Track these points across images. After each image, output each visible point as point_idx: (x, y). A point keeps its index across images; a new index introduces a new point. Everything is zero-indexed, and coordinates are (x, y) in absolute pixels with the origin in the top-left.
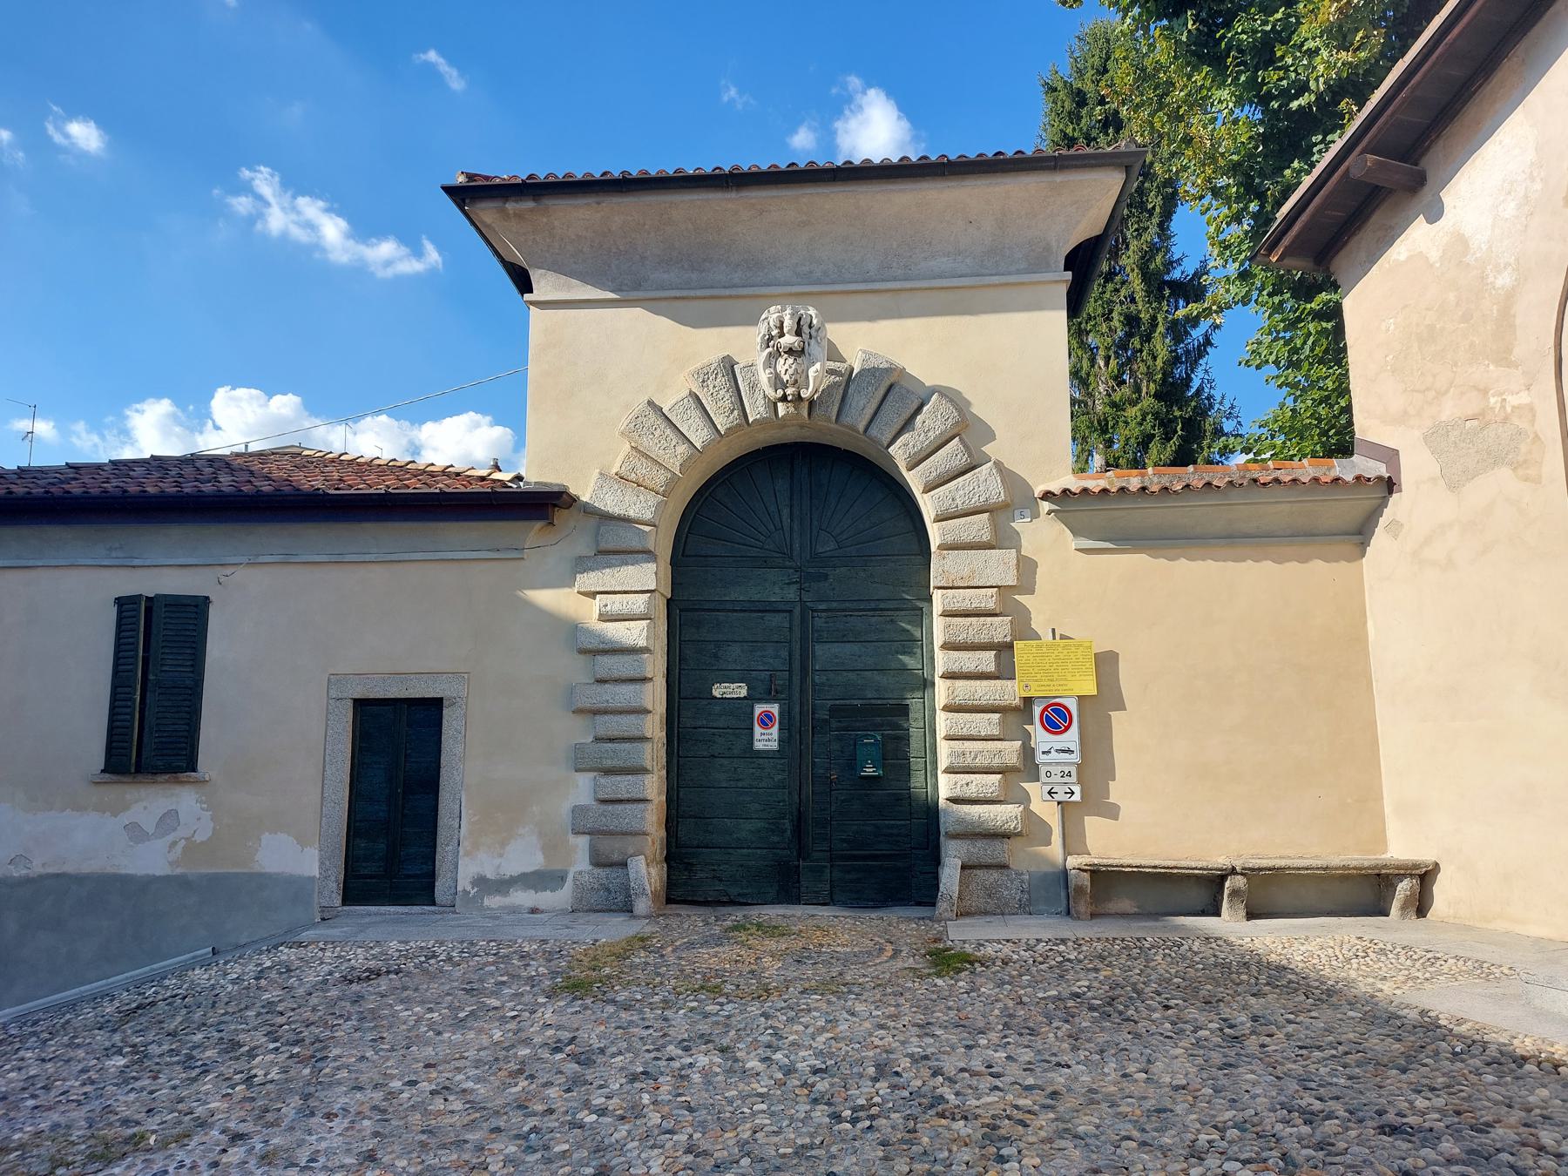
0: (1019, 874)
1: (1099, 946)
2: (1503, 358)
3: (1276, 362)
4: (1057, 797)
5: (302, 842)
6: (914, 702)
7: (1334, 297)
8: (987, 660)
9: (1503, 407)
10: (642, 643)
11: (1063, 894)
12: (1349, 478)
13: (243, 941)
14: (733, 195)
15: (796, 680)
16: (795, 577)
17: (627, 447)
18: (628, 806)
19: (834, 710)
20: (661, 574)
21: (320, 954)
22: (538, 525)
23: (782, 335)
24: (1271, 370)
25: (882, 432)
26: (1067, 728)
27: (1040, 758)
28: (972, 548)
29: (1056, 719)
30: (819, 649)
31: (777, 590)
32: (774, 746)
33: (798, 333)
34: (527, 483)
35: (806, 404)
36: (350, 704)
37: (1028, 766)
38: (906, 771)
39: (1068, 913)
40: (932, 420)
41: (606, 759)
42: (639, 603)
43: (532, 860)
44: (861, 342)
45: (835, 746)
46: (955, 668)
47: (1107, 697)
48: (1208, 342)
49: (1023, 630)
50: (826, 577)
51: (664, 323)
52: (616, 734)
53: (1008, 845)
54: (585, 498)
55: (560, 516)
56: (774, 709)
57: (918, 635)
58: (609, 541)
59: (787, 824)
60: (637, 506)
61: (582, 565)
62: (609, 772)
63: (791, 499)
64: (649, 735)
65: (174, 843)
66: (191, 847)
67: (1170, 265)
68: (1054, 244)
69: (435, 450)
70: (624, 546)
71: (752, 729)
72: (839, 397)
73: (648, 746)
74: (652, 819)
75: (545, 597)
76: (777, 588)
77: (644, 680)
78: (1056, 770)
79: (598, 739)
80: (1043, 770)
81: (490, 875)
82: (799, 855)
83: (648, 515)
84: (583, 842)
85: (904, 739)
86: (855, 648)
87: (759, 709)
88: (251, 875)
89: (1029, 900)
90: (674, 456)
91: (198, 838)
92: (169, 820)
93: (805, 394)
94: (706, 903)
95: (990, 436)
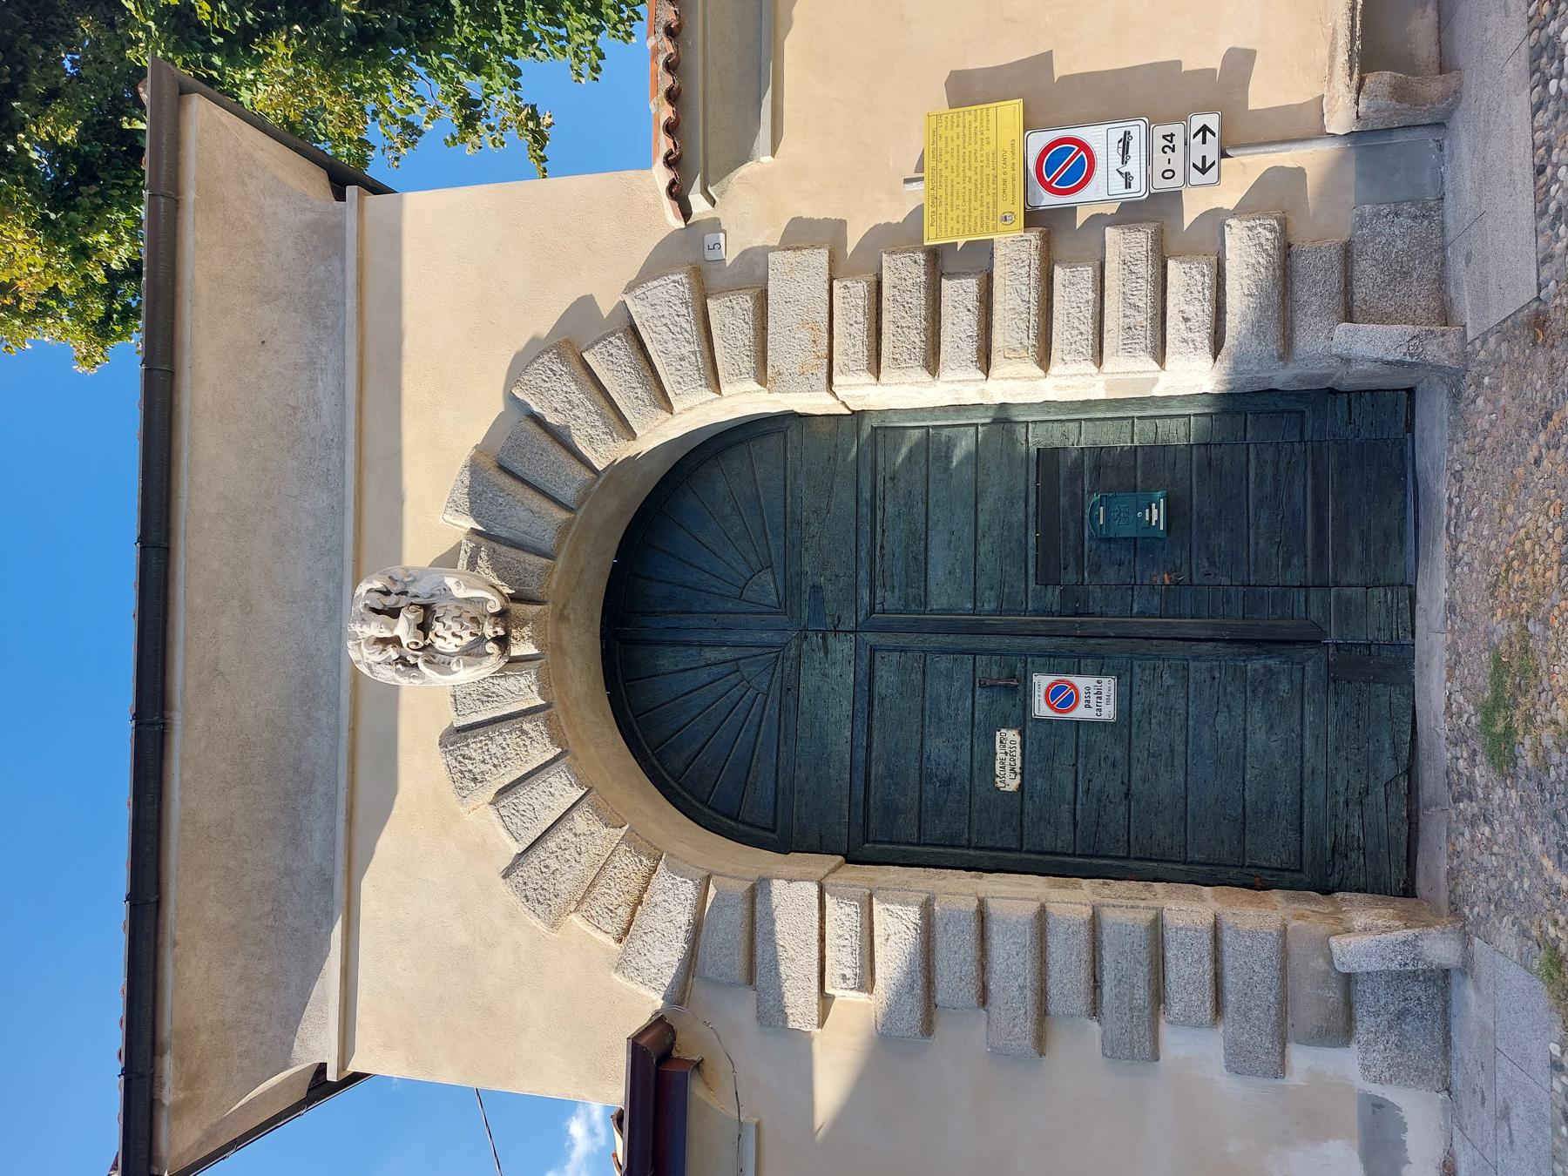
0: (1362, 221)
3: (596, 30)
4: (1212, 156)
6: (1037, 439)
8: (959, 294)
10: (913, 914)
11: (1401, 138)
14: (177, 718)
15: (992, 642)
17: (575, 919)
18: (1228, 962)
19: (1046, 577)
20: (795, 870)
22: (697, 1090)
24: (605, 40)
25: (570, 482)
26: (1083, 146)
27: (1138, 190)
28: (765, 329)
29: (1066, 165)
31: (835, 672)
32: (1108, 684)
33: (394, 613)
35: (516, 608)
37: (1153, 212)
38: (1157, 454)
39: (1440, 125)
40: (556, 399)
41: (1140, 1002)
42: (842, 916)
44: (432, 521)
45: (1111, 575)
46: (970, 349)
47: (1033, 86)
49: (904, 235)
50: (817, 589)
51: (388, 845)
52: (1084, 975)
53: (1302, 239)
54: (658, 1002)
55: (687, 1048)
56: (1042, 682)
57: (917, 434)
58: (730, 959)
59: (1255, 665)
60: (673, 904)
61: (772, 1015)
62: (1158, 996)
63: (688, 644)
64: (1086, 913)
68: (308, 216)
70: (741, 936)
71: (1078, 723)
72: (513, 553)
73: (1109, 916)
74: (1258, 917)
75: (830, 1085)
76: (832, 674)
77: (982, 915)
78: (1160, 161)
79: (1095, 1010)
80: (1160, 184)
82: (1316, 643)
83: (688, 889)
84: (1301, 1058)
85: (1099, 454)
86: (937, 540)
87: (1041, 709)
89: (1413, 202)
90: (593, 837)
93: (495, 605)
94: (1413, 822)
95: (585, 304)
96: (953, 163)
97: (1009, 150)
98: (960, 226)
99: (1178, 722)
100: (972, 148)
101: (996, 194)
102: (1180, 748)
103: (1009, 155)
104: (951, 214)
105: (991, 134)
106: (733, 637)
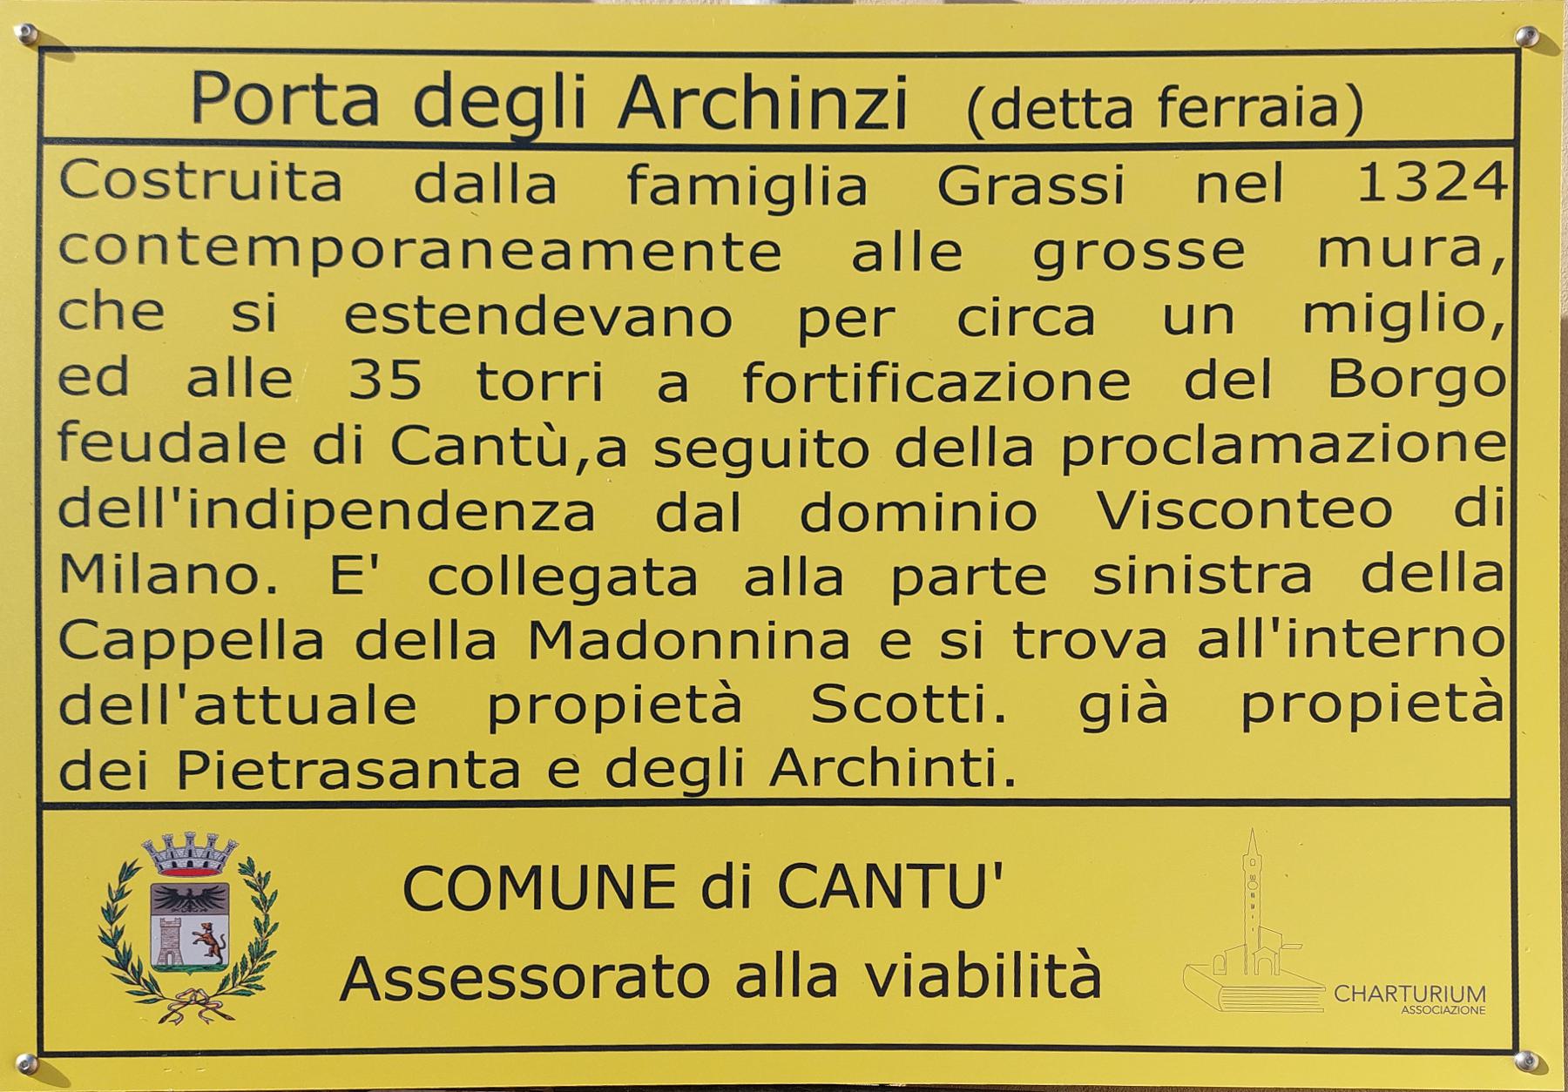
96: (922, 330)
97: (983, 936)
98: (157, 403)
100: (1069, 536)
101: (500, 790)
103: (932, 932)
104: (311, 307)
105: (1201, 741)
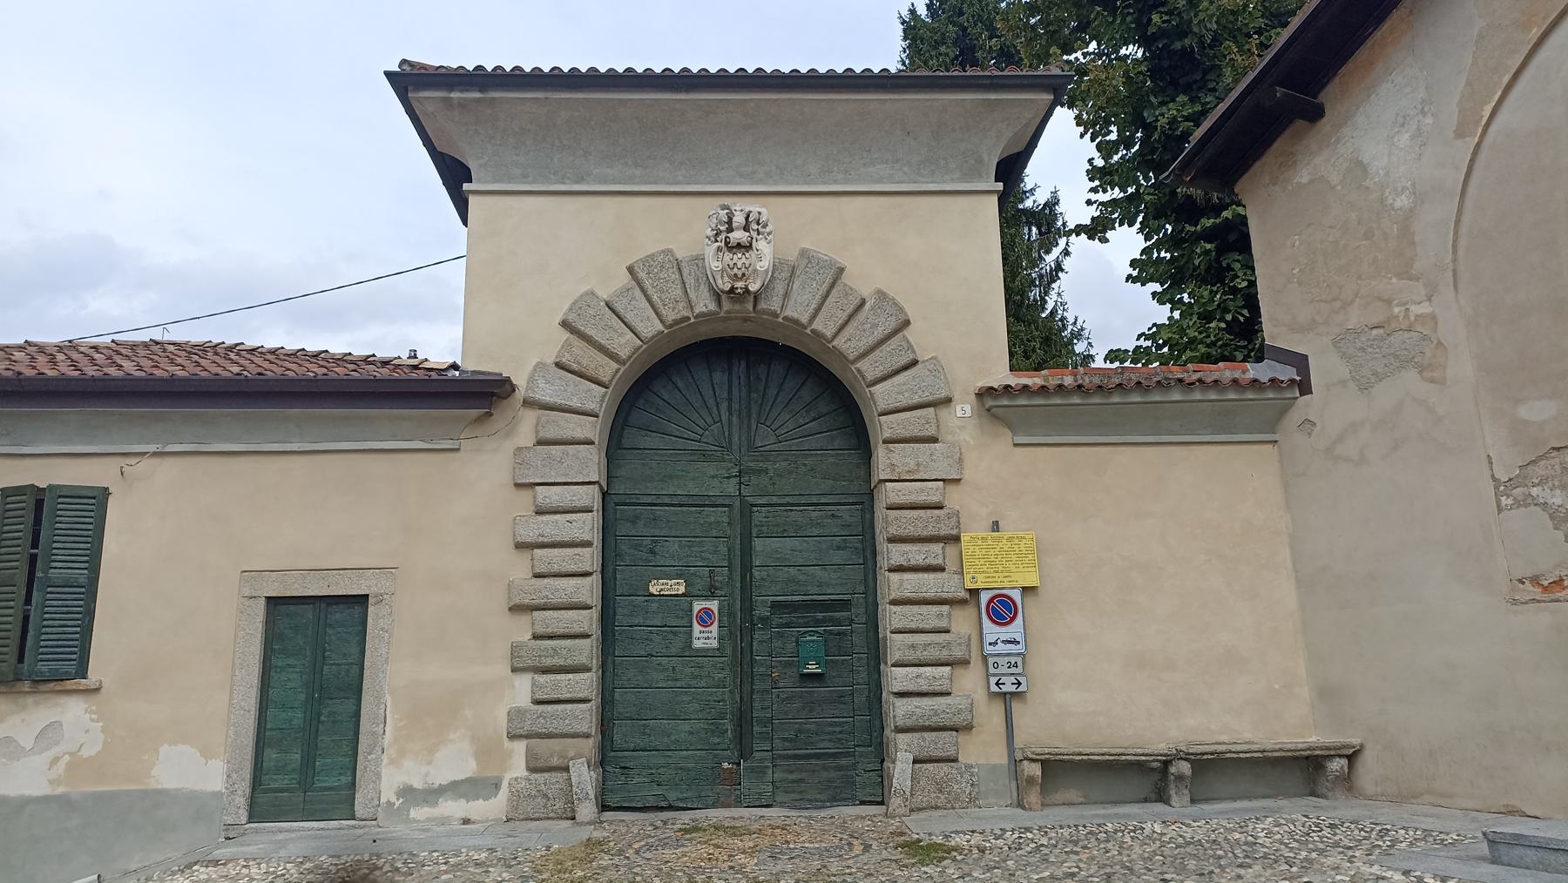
1: (1066, 832)
2: (1405, 274)
5: (207, 754)
7: (1240, 210)
9: (1407, 316)
12: (1264, 379)
13: (133, 867)
16: (735, 471)
21: (245, 871)
23: (730, 230)
26: (1013, 619)
30: (758, 544)
34: (463, 372)
36: (263, 602)
43: (467, 768)
48: (1059, 267)
56: (714, 605)
62: (546, 671)
65: (56, 760)
66: (77, 765)
67: (1024, 195)
69: (1090, 161)
76: (713, 480)
78: (1003, 661)
81: (417, 784)
86: (795, 542)
87: (698, 606)
88: (145, 793)
91: (86, 753)
92: (50, 733)
99: (693, 683)
102: (679, 684)
106: (735, 419)
